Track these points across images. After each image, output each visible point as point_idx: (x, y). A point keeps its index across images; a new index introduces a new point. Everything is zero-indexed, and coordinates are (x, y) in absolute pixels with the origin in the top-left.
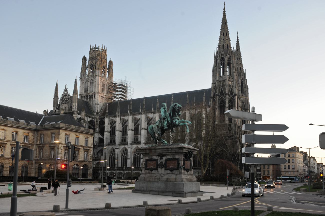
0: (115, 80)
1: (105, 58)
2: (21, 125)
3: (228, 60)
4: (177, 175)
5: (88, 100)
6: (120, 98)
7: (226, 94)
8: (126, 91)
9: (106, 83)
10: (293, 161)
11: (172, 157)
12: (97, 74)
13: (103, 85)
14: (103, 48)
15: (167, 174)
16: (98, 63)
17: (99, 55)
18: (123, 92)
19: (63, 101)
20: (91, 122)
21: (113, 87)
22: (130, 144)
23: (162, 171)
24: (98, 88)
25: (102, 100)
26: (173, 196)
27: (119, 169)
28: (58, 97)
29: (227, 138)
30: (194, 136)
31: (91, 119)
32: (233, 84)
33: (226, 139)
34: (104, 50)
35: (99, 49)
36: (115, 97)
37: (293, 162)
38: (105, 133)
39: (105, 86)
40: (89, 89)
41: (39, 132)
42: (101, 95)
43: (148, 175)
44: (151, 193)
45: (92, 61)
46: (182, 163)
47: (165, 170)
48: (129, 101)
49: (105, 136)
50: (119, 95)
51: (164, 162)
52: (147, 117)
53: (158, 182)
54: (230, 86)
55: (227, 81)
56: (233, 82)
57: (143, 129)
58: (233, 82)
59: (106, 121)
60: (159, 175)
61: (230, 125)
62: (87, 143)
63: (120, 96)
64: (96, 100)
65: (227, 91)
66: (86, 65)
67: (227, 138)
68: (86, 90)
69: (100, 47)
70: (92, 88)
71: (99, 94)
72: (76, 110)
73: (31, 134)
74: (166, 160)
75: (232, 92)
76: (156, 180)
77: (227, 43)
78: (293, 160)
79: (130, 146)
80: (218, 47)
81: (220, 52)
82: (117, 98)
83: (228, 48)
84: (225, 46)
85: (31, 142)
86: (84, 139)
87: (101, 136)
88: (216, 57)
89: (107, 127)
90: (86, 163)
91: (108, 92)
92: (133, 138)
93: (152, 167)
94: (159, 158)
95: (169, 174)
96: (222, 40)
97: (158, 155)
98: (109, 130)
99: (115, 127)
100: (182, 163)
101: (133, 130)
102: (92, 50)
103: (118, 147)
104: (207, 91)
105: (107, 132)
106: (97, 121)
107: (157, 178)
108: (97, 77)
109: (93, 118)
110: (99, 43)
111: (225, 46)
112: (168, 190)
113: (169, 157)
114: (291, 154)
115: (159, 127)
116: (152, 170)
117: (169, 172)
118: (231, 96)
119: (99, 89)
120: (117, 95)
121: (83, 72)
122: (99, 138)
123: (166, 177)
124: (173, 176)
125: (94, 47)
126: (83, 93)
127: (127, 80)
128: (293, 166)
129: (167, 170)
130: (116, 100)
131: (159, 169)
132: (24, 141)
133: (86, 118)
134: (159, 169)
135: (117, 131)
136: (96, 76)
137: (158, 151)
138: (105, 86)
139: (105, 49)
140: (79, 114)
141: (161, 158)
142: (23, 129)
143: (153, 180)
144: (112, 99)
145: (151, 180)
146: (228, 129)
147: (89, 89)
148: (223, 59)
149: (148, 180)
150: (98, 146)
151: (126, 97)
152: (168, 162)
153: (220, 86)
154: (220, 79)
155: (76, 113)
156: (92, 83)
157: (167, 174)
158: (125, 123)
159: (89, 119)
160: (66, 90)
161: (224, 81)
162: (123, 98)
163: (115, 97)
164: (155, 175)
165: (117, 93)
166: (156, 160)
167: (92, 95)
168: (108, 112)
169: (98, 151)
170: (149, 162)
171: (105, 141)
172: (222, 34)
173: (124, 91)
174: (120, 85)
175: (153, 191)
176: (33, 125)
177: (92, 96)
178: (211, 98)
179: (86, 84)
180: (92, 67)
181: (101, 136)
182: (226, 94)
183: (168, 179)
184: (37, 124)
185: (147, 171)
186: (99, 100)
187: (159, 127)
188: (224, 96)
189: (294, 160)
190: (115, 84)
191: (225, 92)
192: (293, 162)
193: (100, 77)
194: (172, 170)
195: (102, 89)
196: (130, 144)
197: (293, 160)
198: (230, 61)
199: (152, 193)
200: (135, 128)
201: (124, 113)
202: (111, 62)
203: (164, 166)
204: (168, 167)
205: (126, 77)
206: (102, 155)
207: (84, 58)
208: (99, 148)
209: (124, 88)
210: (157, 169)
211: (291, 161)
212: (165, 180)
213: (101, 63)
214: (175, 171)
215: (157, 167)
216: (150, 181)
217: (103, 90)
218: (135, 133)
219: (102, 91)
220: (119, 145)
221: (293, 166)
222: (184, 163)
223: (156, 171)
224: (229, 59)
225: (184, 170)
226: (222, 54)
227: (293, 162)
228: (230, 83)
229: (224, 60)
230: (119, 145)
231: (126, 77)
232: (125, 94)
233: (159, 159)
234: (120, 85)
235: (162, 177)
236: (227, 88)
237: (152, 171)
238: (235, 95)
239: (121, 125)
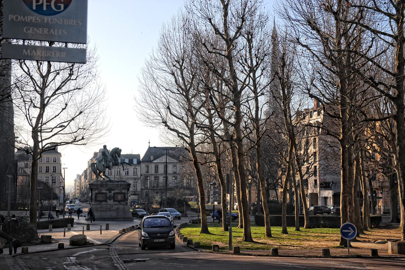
4: (124, 205)
10: (46, 169)
11: (119, 191)
15: (116, 204)
23: (111, 202)
26: (104, 221)
37: (54, 171)
43: (98, 206)
44: (117, 220)
47: (114, 201)
51: (112, 195)
53: (110, 211)
60: (109, 206)
74: (114, 194)
76: (107, 210)
78: (53, 167)
93: (101, 199)
94: (108, 192)
95: (117, 204)
97: (107, 190)
107: (108, 208)
112: (119, 217)
113: (116, 191)
115: (105, 166)
116: (101, 201)
117: (117, 203)
123: (115, 207)
124: (121, 206)
128: (47, 178)
129: (115, 201)
131: (108, 201)
134: (108, 201)
137: (109, 186)
141: (110, 192)
143: (105, 210)
145: (103, 210)
149: (100, 210)
152: (116, 195)
157: (116, 204)
164: (105, 206)
166: (106, 194)
170: (99, 195)
175: (107, 218)
183: (117, 209)
185: (97, 203)
187: (105, 166)
189: (55, 167)
192: (46, 172)
194: (119, 201)
197: (54, 168)
199: (106, 220)
203: (114, 198)
204: (116, 199)
212: (115, 209)
214: (122, 202)
215: (107, 199)
216: (101, 211)
221: (47, 178)
223: (106, 202)
227: (54, 171)
233: (108, 193)
235: (112, 207)
237: (102, 202)
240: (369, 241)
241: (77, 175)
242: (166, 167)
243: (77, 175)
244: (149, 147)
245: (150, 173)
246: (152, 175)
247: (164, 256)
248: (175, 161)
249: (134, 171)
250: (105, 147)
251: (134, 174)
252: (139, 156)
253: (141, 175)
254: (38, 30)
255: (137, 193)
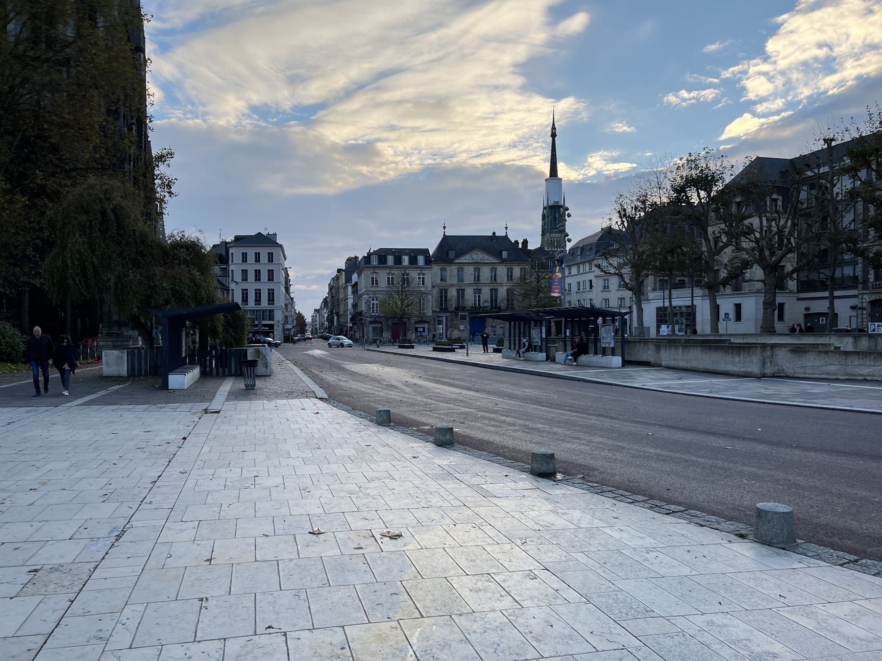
240: (335, 355)
241: (657, 308)
242: (477, 270)
243: (657, 308)
244: (444, 235)
245: (449, 282)
246: (452, 285)
247: (424, 429)
248: (493, 260)
249: (389, 278)
250: (494, 233)
251: (373, 284)
252: (427, 251)
253: (433, 287)
254: (169, 118)
255: (424, 319)
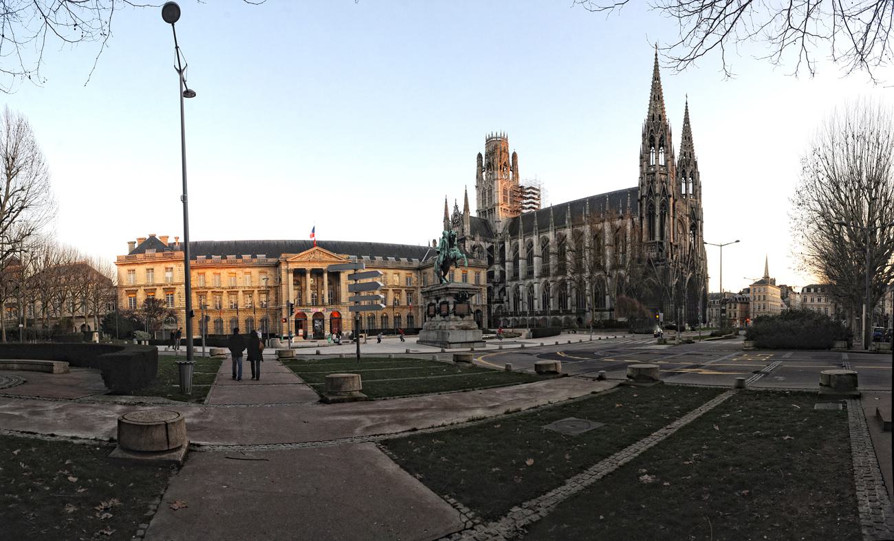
0: (522, 182)
1: (506, 151)
2: (403, 265)
3: (660, 141)
5: (487, 216)
6: (529, 208)
7: (656, 195)
8: (539, 196)
9: (509, 188)
12: (496, 177)
13: (505, 191)
14: (503, 135)
16: (497, 160)
17: (496, 147)
18: (534, 198)
19: (454, 223)
20: (491, 249)
21: (519, 193)
22: (537, 277)
24: (499, 198)
25: (504, 214)
27: (555, 313)
28: (448, 219)
29: (658, 263)
30: (865, 225)
31: (490, 244)
32: (667, 178)
33: (657, 265)
34: (504, 138)
35: (496, 138)
36: (524, 208)
37: (764, 299)
38: (507, 264)
39: (508, 192)
40: (487, 201)
41: (423, 271)
42: (503, 207)
45: (489, 158)
46: (451, 307)
48: (547, 210)
49: (507, 268)
50: (530, 203)
52: (612, 226)
54: (662, 182)
55: (657, 174)
56: (667, 175)
57: (551, 253)
58: (667, 175)
59: (507, 244)
61: (661, 244)
62: (478, 280)
63: (530, 205)
64: (497, 216)
65: (657, 190)
66: (482, 166)
67: (658, 263)
68: (484, 202)
69: (499, 135)
70: (491, 199)
71: (500, 207)
72: (469, 234)
73: (414, 275)
75: (664, 191)
77: (659, 112)
79: (536, 280)
80: (647, 118)
81: (649, 127)
82: (526, 209)
83: (660, 120)
84: (657, 116)
85: (415, 285)
86: (474, 275)
87: (502, 269)
88: (644, 135)
89: (509, 255)
90: (479, 308)
91: (512, 202)
92: (540, 267)
96: (652, 108)
98: (512, 258)
99: (532, 252)
100: (451, 307)
101: (539, 257)
102: (489, 141)
103: (522, 282)
104: (633, 191)
105: (523, 259)
106: (497, 247)
108: (496, 182)
109: (493, 243)
110: (496, 130)
111: (657, 116)
114: (762, 288)
118: (664, 198)
119: (500, 198)
120: (526, 204)
121: (479, 178)
122: (501, 271)
125: (491, 136)
126: (481, 208)
127: (538, 179)
130: (525, 211)
132: (407, 284)
133: (482, 243)
135: (535, 256)
136: (494, 180)
138: (508, 192)
139: (506, 137)
140: (473, 239)
142: (405, 269)
144: (518, 211)
146: (658, 249)
147: (487, 201)
148: (652, 139)
150: (500, 283)
151: (539, 205)
153: (648, 182)
154: (649, 171)
155: (468, 238)
156: (490, 191)
158: (563, 240)
159: (488, 245)
160: (456, 207)
161: (654, 174)
162: (534, 208)
163: (524, 208)
165: (525, 201)
167: (491, 209)
168: (536, 224)
169: (500, 289)
171: (507, 275)
172: (653, 97)
173: (536, 197)
174: (528, 189)
176: (416, 262)
177: (492, 211)
178: (639, 200)
179: (484, 194)
180: (490, 166)
181: (502, 269)
182: (656, 195)
184: (420, 260)
186: (500, 215)
188: (653, 198)
190: (521, 187)
191: (655, 192)
193: (499, 181)
195: (504, 197)
196: (537, 277)
198: (663, 141)
200: (543, 253)
201: (543, 227)
202: (514, 155)
205: (536, 176)
206: (505, 295)
207: (480, 156)
208: (501, 286)
209: (534, 192)
210: (435, 316)
211: (762, 298)
213: (501, 158)
217: (505, 200)
218: (543, 260)
219: (504, 200)
220: (524, 279)
222: (455, 307)
224: (661, 138)
225: (455, 315)
226: (652, 131)
227: (764, 299)
228: (663, 177)
229: (654, 141)
230: (524, 279)
231: (536, 176)
232: (537, 202)
234: (528, 189)
236: (657, 185)
238: (670, 196)
239: (525, 250)
